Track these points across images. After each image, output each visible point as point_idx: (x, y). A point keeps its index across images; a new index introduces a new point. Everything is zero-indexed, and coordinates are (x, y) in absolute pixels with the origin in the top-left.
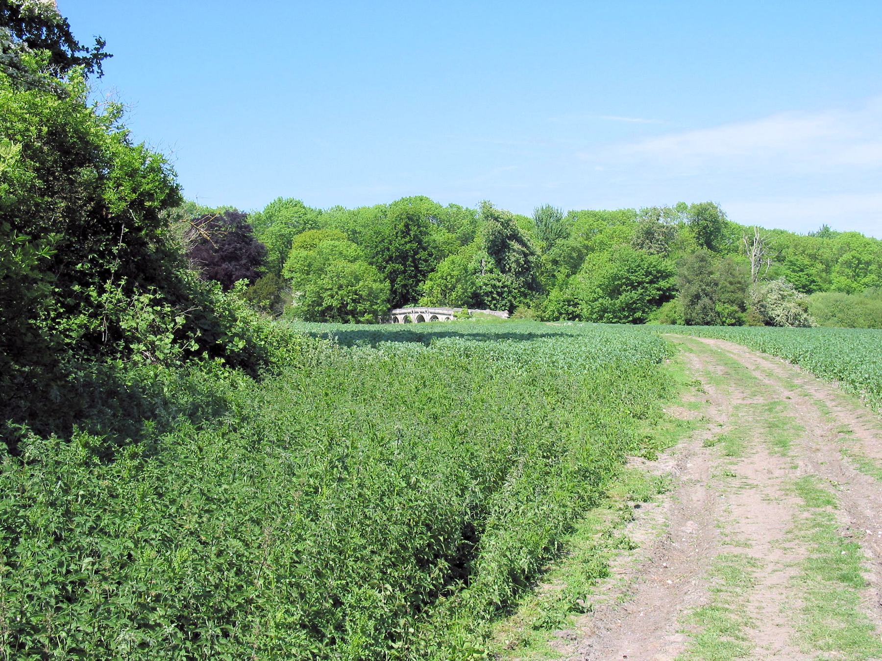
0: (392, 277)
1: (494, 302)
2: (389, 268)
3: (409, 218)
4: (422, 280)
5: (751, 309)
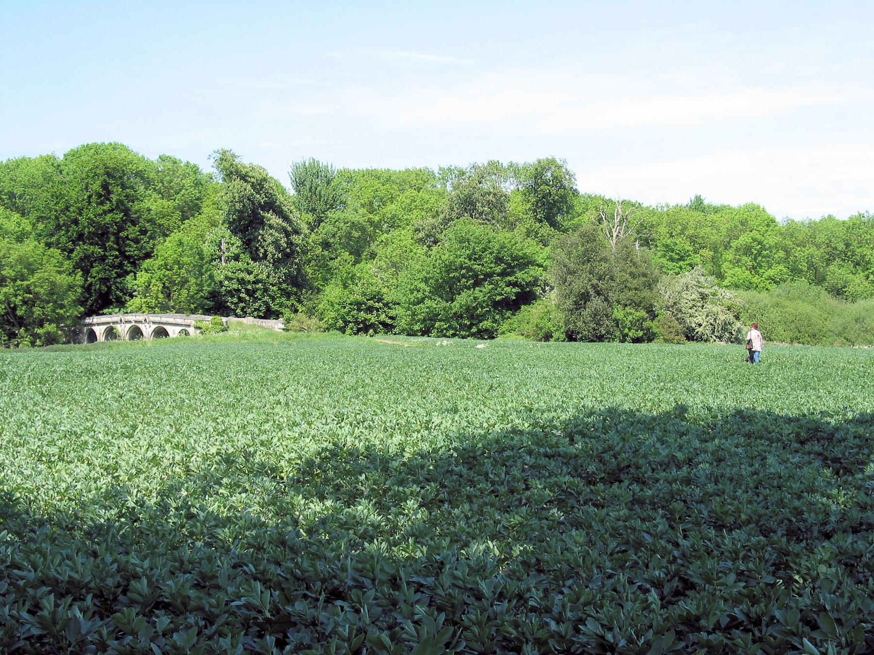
0: (85, 265)
1: (242, 305)
2: (79, 252)
3: (108, 174)
4: (131, 271)
5: (664, 315)
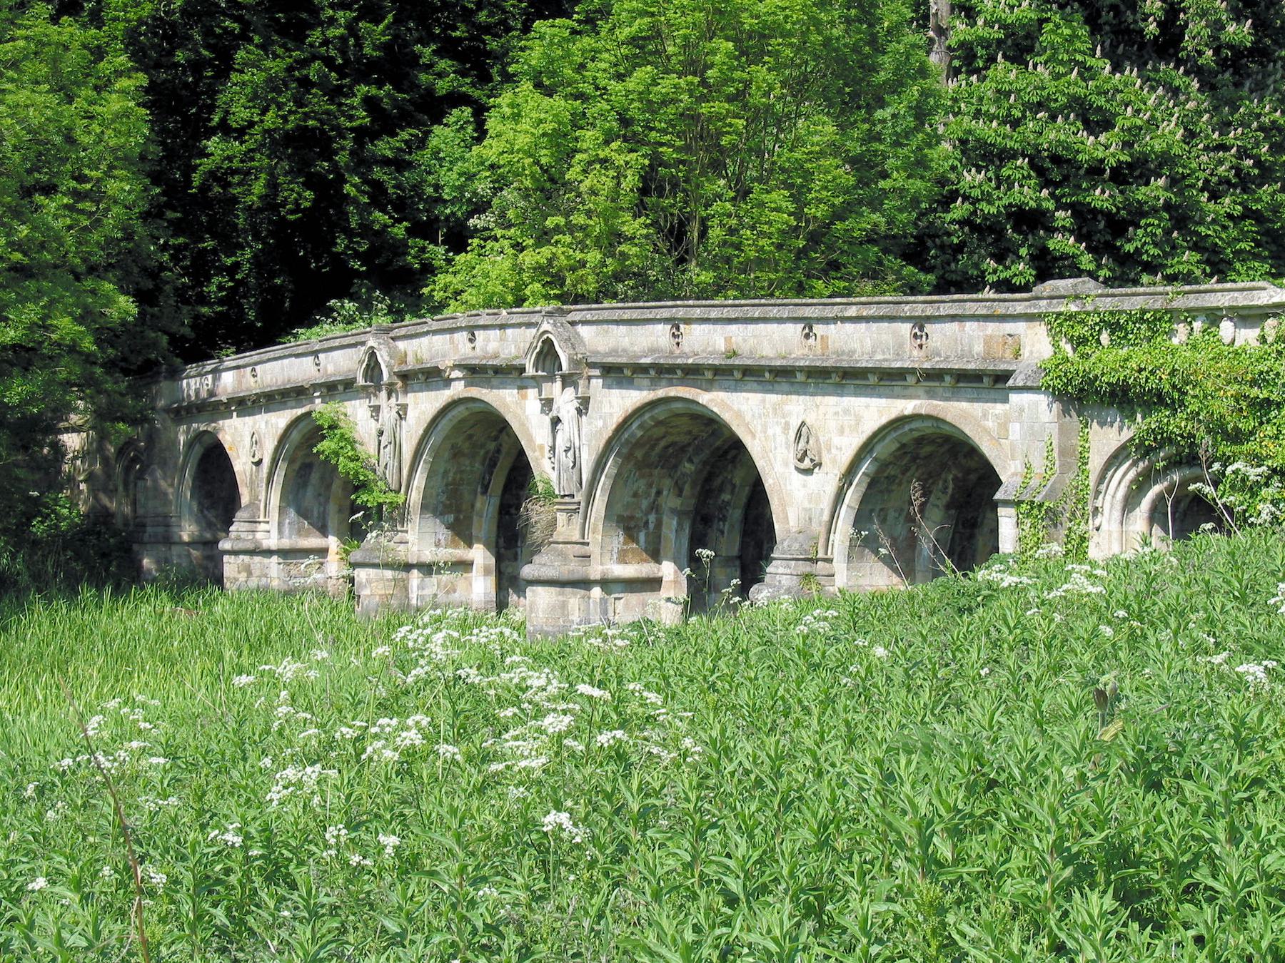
4: (456, 99)
